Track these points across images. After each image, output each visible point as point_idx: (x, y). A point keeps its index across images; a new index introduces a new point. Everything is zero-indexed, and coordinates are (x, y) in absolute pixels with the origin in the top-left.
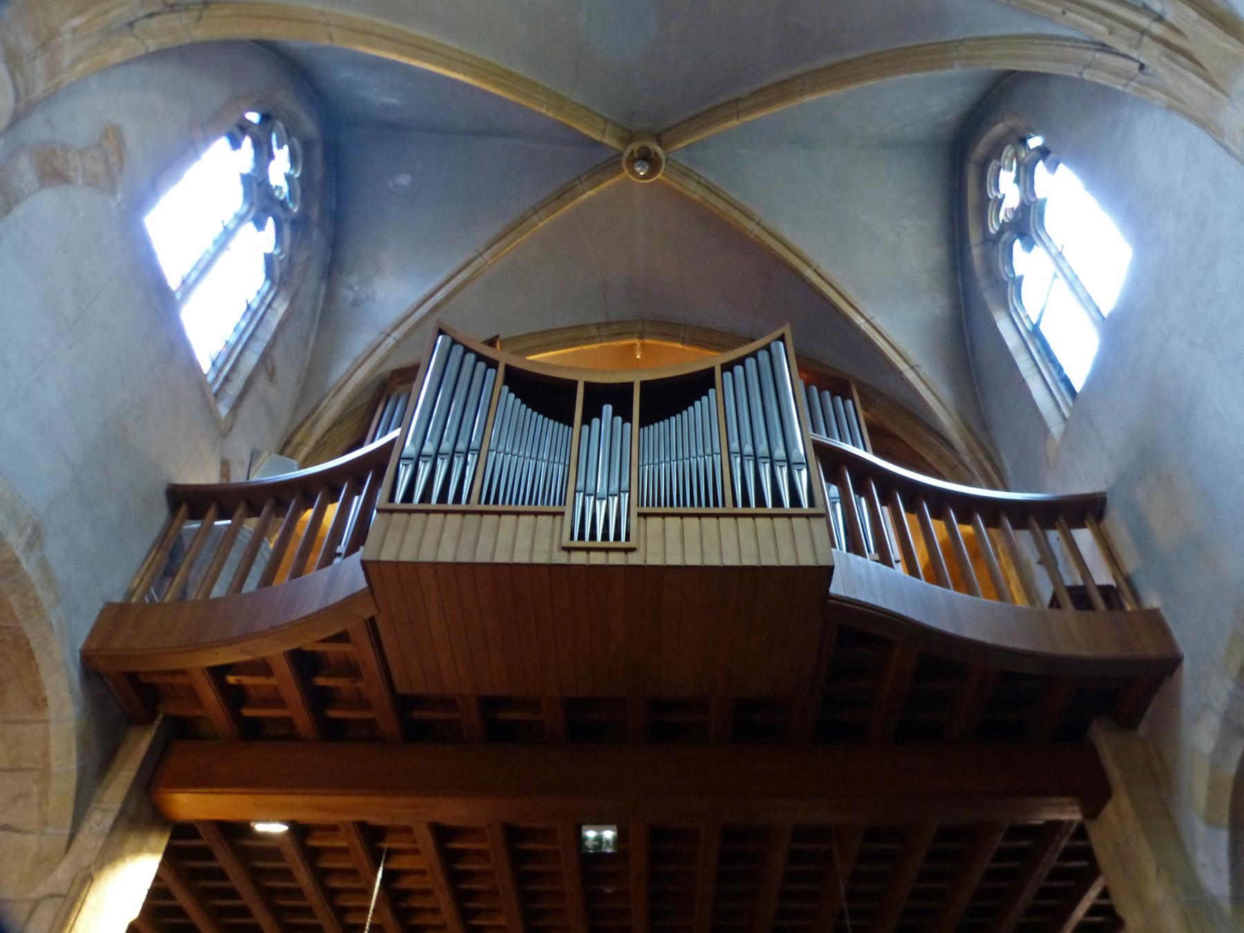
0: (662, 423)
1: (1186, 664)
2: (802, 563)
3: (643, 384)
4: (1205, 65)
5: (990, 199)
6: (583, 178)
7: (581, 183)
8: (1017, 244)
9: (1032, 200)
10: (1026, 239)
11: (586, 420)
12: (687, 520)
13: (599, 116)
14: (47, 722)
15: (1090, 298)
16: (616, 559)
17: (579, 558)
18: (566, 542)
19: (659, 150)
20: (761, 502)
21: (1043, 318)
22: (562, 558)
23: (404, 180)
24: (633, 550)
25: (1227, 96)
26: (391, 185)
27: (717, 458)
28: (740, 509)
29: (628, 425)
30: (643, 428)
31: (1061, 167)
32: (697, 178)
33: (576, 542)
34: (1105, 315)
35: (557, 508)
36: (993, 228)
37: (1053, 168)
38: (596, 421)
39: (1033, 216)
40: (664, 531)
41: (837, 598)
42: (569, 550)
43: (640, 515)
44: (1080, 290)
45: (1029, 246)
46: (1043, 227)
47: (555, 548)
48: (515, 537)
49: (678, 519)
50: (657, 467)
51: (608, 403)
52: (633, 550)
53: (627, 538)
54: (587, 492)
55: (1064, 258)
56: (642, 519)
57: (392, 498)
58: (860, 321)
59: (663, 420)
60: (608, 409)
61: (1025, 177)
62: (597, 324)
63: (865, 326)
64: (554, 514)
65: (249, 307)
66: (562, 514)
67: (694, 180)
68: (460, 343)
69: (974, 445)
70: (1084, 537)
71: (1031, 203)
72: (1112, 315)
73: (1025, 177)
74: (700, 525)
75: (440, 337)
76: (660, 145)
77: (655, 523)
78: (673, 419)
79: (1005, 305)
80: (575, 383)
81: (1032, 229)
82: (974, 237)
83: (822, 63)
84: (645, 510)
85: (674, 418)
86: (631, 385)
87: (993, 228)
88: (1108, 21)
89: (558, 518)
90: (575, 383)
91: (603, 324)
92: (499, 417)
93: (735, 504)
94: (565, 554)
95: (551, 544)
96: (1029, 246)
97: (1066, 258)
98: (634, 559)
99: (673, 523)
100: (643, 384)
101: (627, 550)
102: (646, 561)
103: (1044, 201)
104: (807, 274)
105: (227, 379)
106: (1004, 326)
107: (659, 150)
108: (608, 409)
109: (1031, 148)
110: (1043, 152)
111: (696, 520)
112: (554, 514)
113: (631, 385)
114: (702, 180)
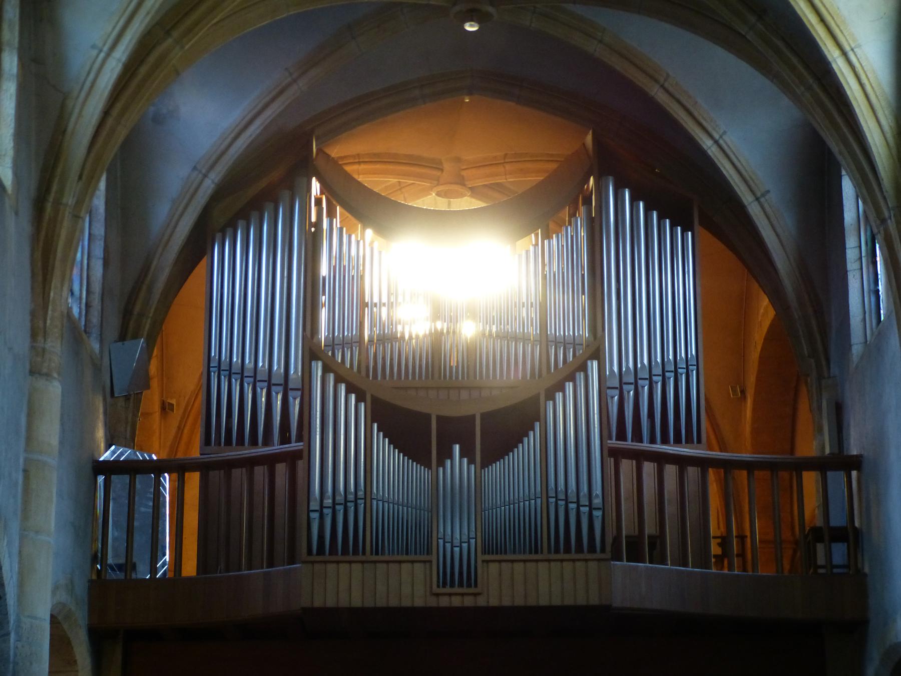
2: (516, 604)
11: (441, 463)
13: (397, 190)
14: (77, 671)
16: (468, 602)
17: (444, 602)
22: (432, 602)
24: (479, 594)
27: (539, 501)
29: (473, 467)
30: (499, 461)
40: (500, 575)
47: (428, 594)
50: (494, 511)
52: (479, 594)
57: (310, 552)
64: (425, 562)
84: (487, 557)
85: (507, 457)
89: (428, 565)
92: (865, 112)
98: (481, 602)
101: (475, 595)
104: (652, 94)
105: (88, 306)
112: (425, 562)
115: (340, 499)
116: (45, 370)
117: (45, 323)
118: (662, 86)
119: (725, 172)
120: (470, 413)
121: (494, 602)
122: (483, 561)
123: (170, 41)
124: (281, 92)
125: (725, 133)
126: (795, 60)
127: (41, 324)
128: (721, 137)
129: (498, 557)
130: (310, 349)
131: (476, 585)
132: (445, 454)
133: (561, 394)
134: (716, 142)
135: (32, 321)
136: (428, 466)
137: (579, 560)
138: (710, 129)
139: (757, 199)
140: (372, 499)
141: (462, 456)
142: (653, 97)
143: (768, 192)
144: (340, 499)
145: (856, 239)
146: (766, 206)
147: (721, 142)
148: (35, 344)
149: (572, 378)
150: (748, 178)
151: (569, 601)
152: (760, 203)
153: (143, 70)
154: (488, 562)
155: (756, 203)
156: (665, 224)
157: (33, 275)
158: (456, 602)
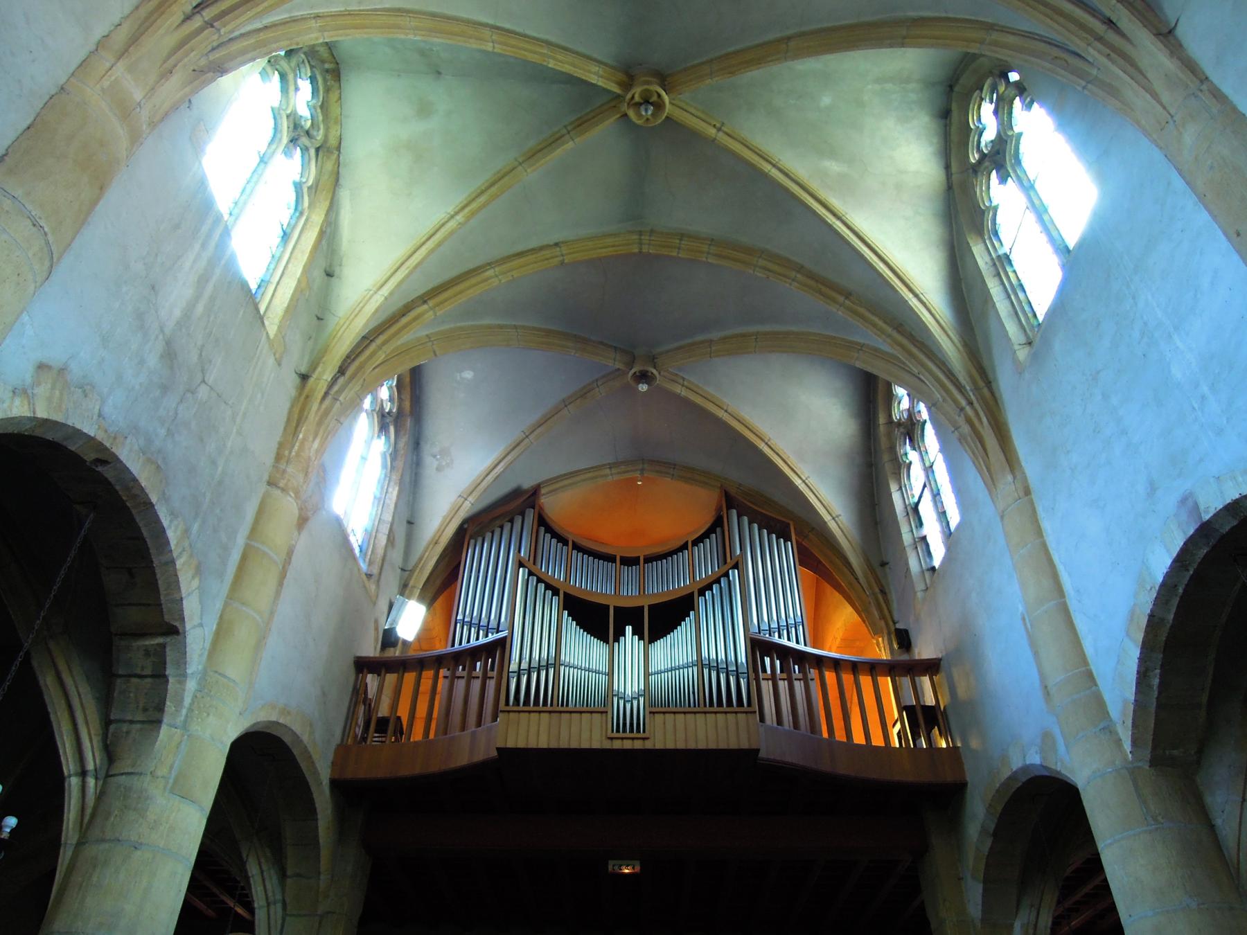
0: (662, 640)
1: (969, 785)
3: (650, 606)
4: (990, 455)
5: (971, 129)
6: (599, 383)
7: (598, 387)
8: (1017, 103)
9: (1010, 133)
10: (1002, 171)
11: (617, 640)
12: (677, 715)
15: (944, 513)
16: (638, 745)
17: (617, 745)
18: (610, 734)
19: (654, 371)
20: (720, 703)
21: (922, 499)
22: (607, 745)
23: (468, 375)
24: (647, 738)
25: (995, 488)
26: (458, 378)
28: (708, 709)
31: (1035, 105)
32: (681, 381)
33: (615, 735)
34: (1071, 244)
35: (602, 709)
36: (974, 157)
37: (1028, 107)
38: (622, 639)
39: (1010, 149)
41: (763, 759)
42: (612, 739)
43: (650, 713)
44: (939, 505)
45: (1003, 180)
46: (923, 440)
47: (604, 738)
48: (581, 730)
49: (672, 715)
51: (629, 625)
52: (647, 738)
53: (644, 731)
54: (620, 696)
55: (933, 472)
56: (652, 715)
57: (507, 703)
58: (798, 482)
59: (663, 638)
60: (629, 629)
61: (1003, 110)
62: (609, 464)
63: (802, 487)
64: (602, 712)
65: (273, 256)
66: (607, 712)
67: (680, 384)
68: (535, 575)
69: (873, 581)
70: (926, 681)
71: (1008, 136)
72: (1081, 244)
73: (1003, 110)
74: (685, 719)
75: (521, 569)
76: (655, 368)
77: (659, 717)
78: (668, 636)
79: (899, 480)
80: (608, 607)
81: (1008, 162)
82: (882, 420)
83: (767, 328)
84: (654, 710)
86: (643, 607)
87: (974, 157)
88: (945, 394)
89: (604, 715)
90: (608, 607)
91: (614, 463)
93: (705, 706)
94: (610, 741)
95: (601, 734)
96: (1003, 180)
97: (1013, 262)
98: (648, 745)
99: (669, 717)
100: (650, 606)
101: (644, 739)
102: (654, 746)
103: (1020, 135)
104: (761, 448)
106: (896, 497)
107: (654, 371)
108: (629, 629)
109: (1011, 81)
110: (1020, 88)
111: (683, 715)
112: (602, 712)
113: (643, 607)
114: (686, 383)
115: (534, 664)
116: (281, 485)
117: (290, 453)
118: (766, 444)
119: (811, 500)
120: (637, 555)
121: (659, 746)
122: (650, 713)
123: (425, 307)
124: (518, 444)
125: (809, 477)
126: (876, 319)
127: (287, 453)
128: (807, 479)
129: (663, 709)
130: (520, 561)
131: (644, 731)
132: (620, 633)
133: (714, 535)
134: (804, 481)
135: (278, 449)
136: (606, 641)
137: (729, 712)
138: (799, 473)
139: (833, 519)
140: (560, 665)
141: (634, 634)
142: (761, 450)
143: (840, 515)
144: (534, 664)
145: (908, 527)
146: (839, 523)
147: (807, 481)
148: (277, 465)
149: (718, 581)
150: (826, 504)
151: (723, 746)
152: (835, 520)
153: (404, 320)
154: (654, 713)
155: (833, 521)
156: (772, 538)
157: (289, 420)
158: (628, 745)
